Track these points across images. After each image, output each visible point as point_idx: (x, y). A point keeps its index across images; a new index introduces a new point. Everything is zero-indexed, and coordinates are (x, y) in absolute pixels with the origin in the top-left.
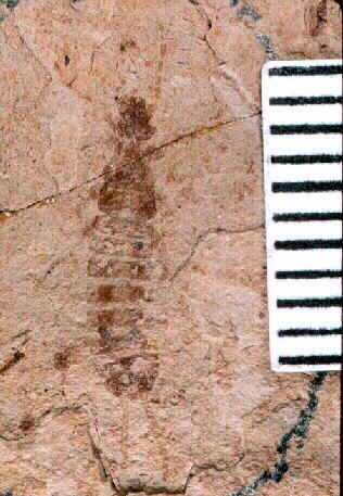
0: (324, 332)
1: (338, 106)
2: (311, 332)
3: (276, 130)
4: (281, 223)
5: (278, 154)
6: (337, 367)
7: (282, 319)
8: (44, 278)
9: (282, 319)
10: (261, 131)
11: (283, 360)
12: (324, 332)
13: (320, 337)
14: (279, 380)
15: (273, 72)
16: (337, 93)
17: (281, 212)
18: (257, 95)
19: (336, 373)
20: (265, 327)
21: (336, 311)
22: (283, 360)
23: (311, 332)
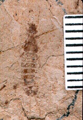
0: (78, 80)
1: (82, 26)
2: (75, 80)
3: (67, 31)
4: (68, 54)
5: (67, 37)
6: (81, 89)
7: (68, 77)
8: (11, 67)
9: (68, 77)
10: (63, 32)
11: (69, 87)
12: (78, 80)
13: (77, 82)
14: (68, 92)
15: (66, 17)
16: (82, 23)
17: (68, 51)
18: (62, 23)
19: (81, 90)
20: (64, 79)
21: (81, 75)
22: (69, 87)
23: (75, 80)
